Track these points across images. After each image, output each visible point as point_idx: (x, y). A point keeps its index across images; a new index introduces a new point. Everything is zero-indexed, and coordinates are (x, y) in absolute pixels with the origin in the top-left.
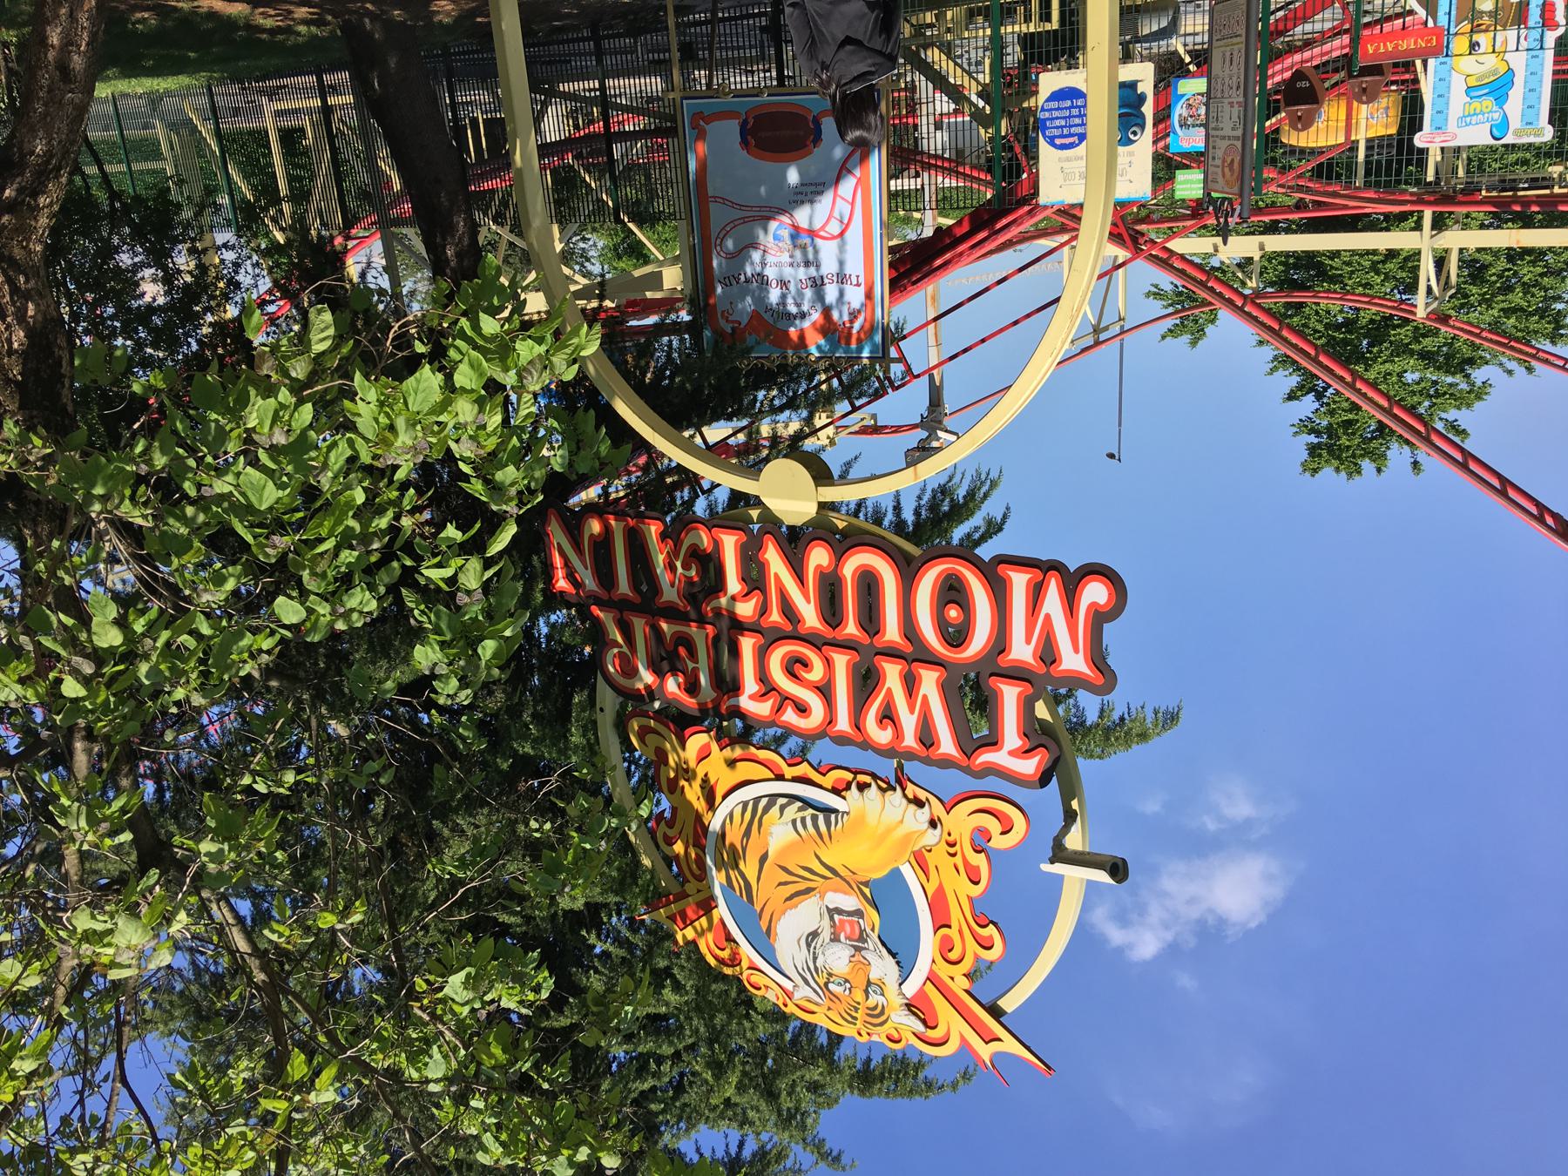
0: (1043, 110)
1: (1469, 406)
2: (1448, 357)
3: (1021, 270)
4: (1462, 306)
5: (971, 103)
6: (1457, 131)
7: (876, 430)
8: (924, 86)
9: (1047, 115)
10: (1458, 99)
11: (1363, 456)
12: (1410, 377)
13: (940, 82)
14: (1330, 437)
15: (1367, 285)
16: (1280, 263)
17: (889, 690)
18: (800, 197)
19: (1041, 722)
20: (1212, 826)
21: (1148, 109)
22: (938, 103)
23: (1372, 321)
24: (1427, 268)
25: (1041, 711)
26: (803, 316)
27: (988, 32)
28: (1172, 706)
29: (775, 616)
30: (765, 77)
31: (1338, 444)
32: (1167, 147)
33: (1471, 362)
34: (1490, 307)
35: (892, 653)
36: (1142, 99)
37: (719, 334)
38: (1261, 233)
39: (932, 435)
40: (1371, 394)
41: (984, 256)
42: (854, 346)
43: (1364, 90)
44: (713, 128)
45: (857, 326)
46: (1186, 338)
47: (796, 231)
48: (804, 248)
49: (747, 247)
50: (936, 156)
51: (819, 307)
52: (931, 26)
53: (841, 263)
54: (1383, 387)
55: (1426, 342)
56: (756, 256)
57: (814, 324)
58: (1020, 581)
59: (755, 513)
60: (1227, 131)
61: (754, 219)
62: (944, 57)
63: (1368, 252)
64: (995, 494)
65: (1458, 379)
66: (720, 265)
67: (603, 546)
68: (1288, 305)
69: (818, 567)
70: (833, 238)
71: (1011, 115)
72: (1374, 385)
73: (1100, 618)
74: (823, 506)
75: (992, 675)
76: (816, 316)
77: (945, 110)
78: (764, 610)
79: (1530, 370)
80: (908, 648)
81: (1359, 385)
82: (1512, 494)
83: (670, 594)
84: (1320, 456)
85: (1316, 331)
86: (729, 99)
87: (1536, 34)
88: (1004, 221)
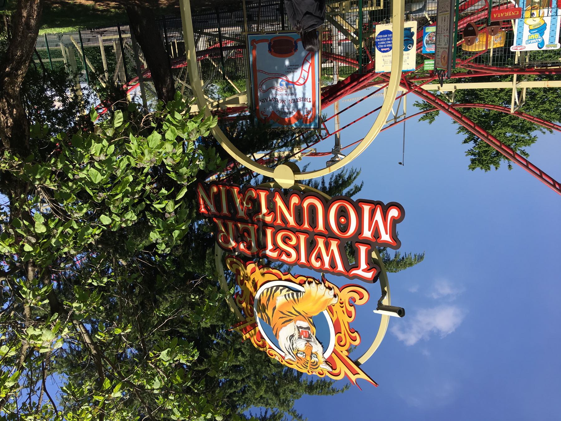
0: (377, 38)
1: (529, 145)
2: (522, 127)
3: (350, 107)
4: (527, 109)
5: (351, 36)
6: (526, 46)
7: (316, 154)
8: (335, 30)
9: (378, 40)
10: (526, 33)
11: (491, 163)
12: (508, 135)
13: (340, 28)
14: (479, 156)
15: (493, 101)
16: (462, 93)
17: (320, 248)
18: (289, 70)
19: (374, 259)
20: (435, 296)
21: (415, 38)
22: (339, 36)
23: (495, 114)
24: (515, 95)
25: (374, 255)
26: (290, 113)
27: (358, 10)
28: (421, 253)
29: (279, 221)
30: (277, 27)
31: (482, 159)
32: (421, 51)
33: (530, 129)
34: (537, 109)
35: (321, 235)
36: (413, 34)
37: (260, 120)
38: (455, 83)
39: (336, 156)
40: (494, 141)
41: (356, 91)
42: (308, 124)
43: (493, 30)
44: (259, 45)
45: (309, 116)
46: (428, 121)
47: (288, 82)
48: (291, 89)
49: (270, 88)
50: (338, 55)
51: (296, 110)
52: (337, 8)
53: (304, 94)
54: (498, 138)
55: (514, 122)
56: (274, 92)
57: (294, 116)
58: (366, 209)
59: (272, 184)
60: (443, 46)
61: (273, 78)
62: (342, 19)
63: (494, 89)
64: (358, 177)
65: (525, 135)
66: (261, 95)
67: (218, 196)
68: (464, 109)
69: (295, 204)
70: (301, 85)
71: (365, 40)
72: (495, 138)
73: (395, 221)
74: (296, 182)
75: (356, 242)
76: (294, 113)
77: (342, 38)
78: (275, 219)
79: (551, 132)
80: (327, 233)
81: (489, 138)
82: (544, 177)
83: (241, 214)
84: (475, 163)
85: (474, 118)
86: (265, 35)
87: (554, 10)
88: (363, 79)
